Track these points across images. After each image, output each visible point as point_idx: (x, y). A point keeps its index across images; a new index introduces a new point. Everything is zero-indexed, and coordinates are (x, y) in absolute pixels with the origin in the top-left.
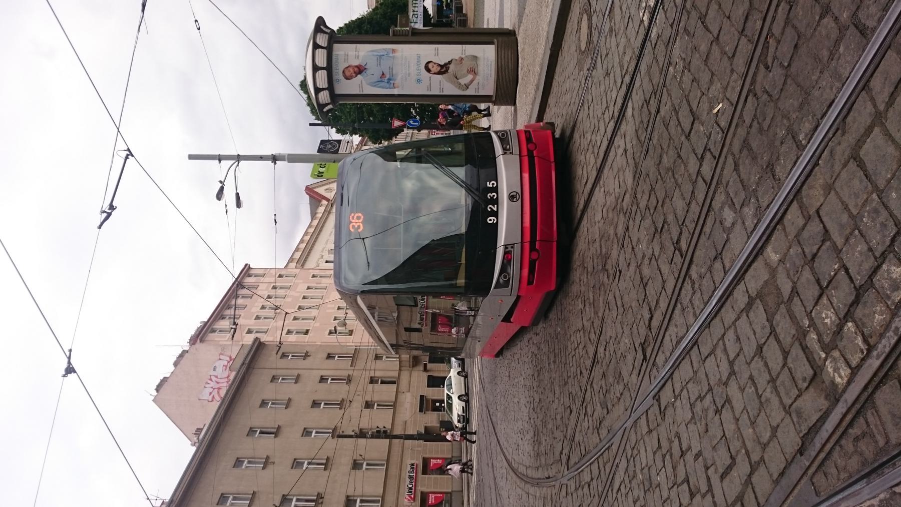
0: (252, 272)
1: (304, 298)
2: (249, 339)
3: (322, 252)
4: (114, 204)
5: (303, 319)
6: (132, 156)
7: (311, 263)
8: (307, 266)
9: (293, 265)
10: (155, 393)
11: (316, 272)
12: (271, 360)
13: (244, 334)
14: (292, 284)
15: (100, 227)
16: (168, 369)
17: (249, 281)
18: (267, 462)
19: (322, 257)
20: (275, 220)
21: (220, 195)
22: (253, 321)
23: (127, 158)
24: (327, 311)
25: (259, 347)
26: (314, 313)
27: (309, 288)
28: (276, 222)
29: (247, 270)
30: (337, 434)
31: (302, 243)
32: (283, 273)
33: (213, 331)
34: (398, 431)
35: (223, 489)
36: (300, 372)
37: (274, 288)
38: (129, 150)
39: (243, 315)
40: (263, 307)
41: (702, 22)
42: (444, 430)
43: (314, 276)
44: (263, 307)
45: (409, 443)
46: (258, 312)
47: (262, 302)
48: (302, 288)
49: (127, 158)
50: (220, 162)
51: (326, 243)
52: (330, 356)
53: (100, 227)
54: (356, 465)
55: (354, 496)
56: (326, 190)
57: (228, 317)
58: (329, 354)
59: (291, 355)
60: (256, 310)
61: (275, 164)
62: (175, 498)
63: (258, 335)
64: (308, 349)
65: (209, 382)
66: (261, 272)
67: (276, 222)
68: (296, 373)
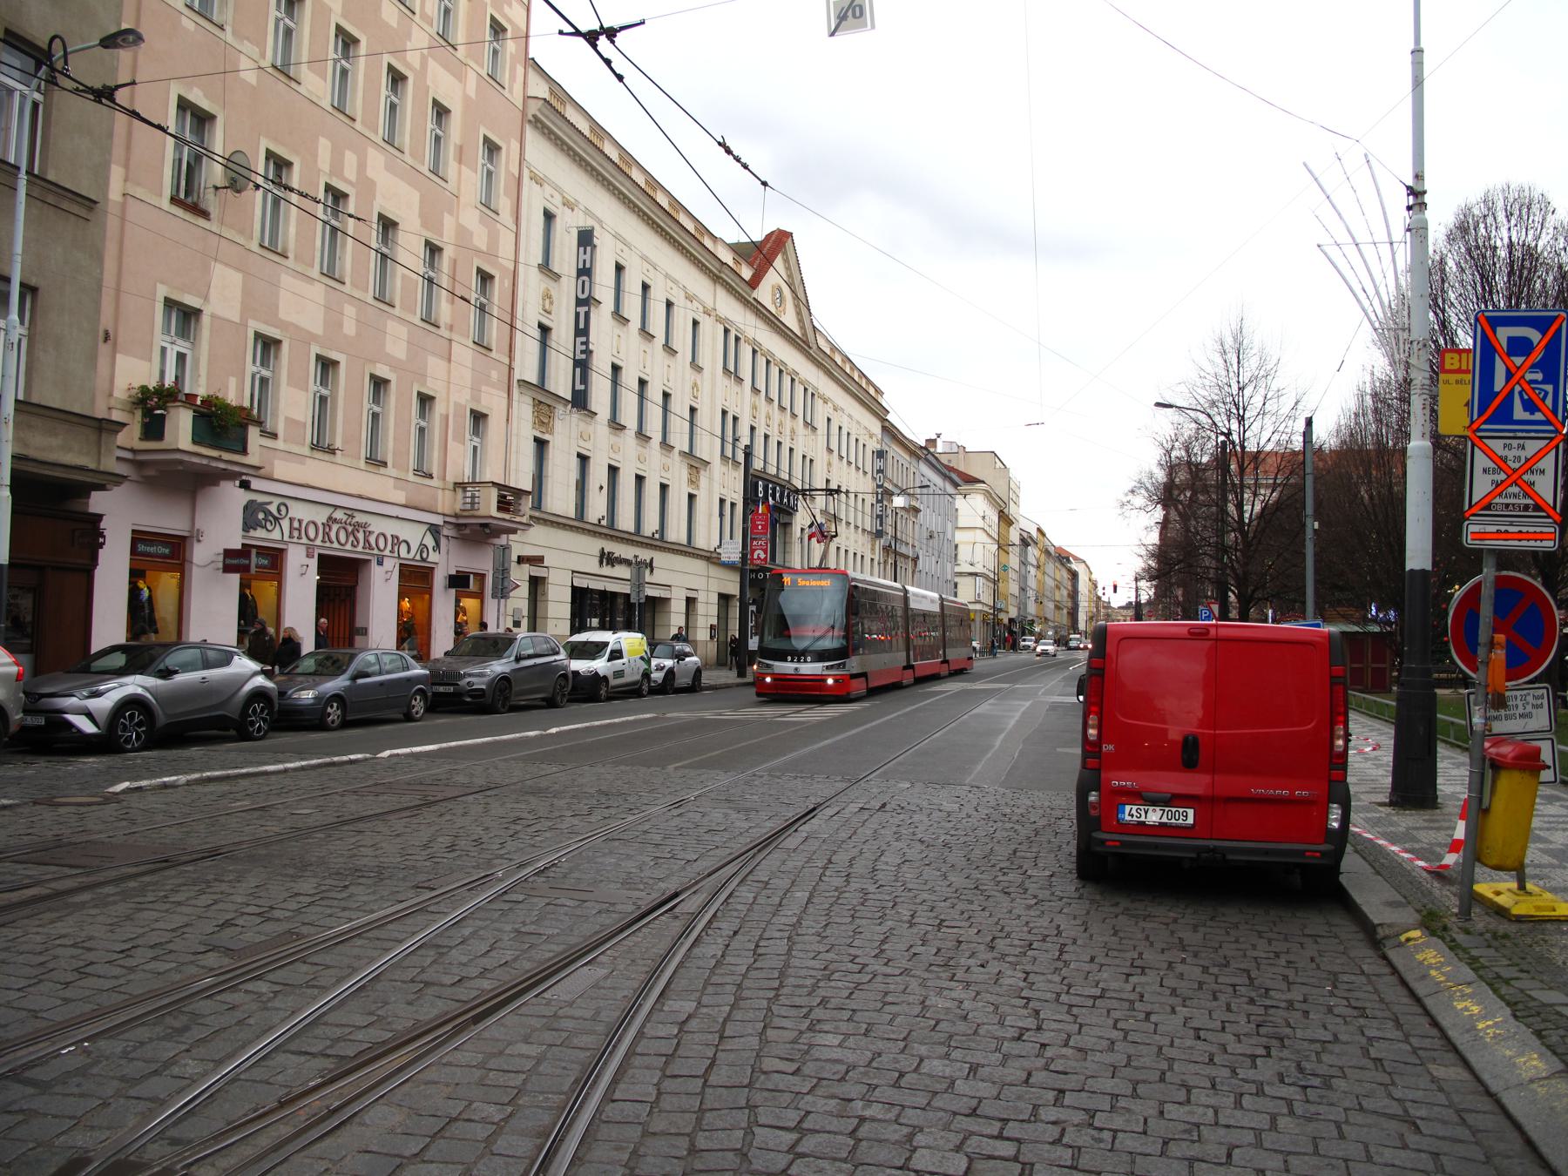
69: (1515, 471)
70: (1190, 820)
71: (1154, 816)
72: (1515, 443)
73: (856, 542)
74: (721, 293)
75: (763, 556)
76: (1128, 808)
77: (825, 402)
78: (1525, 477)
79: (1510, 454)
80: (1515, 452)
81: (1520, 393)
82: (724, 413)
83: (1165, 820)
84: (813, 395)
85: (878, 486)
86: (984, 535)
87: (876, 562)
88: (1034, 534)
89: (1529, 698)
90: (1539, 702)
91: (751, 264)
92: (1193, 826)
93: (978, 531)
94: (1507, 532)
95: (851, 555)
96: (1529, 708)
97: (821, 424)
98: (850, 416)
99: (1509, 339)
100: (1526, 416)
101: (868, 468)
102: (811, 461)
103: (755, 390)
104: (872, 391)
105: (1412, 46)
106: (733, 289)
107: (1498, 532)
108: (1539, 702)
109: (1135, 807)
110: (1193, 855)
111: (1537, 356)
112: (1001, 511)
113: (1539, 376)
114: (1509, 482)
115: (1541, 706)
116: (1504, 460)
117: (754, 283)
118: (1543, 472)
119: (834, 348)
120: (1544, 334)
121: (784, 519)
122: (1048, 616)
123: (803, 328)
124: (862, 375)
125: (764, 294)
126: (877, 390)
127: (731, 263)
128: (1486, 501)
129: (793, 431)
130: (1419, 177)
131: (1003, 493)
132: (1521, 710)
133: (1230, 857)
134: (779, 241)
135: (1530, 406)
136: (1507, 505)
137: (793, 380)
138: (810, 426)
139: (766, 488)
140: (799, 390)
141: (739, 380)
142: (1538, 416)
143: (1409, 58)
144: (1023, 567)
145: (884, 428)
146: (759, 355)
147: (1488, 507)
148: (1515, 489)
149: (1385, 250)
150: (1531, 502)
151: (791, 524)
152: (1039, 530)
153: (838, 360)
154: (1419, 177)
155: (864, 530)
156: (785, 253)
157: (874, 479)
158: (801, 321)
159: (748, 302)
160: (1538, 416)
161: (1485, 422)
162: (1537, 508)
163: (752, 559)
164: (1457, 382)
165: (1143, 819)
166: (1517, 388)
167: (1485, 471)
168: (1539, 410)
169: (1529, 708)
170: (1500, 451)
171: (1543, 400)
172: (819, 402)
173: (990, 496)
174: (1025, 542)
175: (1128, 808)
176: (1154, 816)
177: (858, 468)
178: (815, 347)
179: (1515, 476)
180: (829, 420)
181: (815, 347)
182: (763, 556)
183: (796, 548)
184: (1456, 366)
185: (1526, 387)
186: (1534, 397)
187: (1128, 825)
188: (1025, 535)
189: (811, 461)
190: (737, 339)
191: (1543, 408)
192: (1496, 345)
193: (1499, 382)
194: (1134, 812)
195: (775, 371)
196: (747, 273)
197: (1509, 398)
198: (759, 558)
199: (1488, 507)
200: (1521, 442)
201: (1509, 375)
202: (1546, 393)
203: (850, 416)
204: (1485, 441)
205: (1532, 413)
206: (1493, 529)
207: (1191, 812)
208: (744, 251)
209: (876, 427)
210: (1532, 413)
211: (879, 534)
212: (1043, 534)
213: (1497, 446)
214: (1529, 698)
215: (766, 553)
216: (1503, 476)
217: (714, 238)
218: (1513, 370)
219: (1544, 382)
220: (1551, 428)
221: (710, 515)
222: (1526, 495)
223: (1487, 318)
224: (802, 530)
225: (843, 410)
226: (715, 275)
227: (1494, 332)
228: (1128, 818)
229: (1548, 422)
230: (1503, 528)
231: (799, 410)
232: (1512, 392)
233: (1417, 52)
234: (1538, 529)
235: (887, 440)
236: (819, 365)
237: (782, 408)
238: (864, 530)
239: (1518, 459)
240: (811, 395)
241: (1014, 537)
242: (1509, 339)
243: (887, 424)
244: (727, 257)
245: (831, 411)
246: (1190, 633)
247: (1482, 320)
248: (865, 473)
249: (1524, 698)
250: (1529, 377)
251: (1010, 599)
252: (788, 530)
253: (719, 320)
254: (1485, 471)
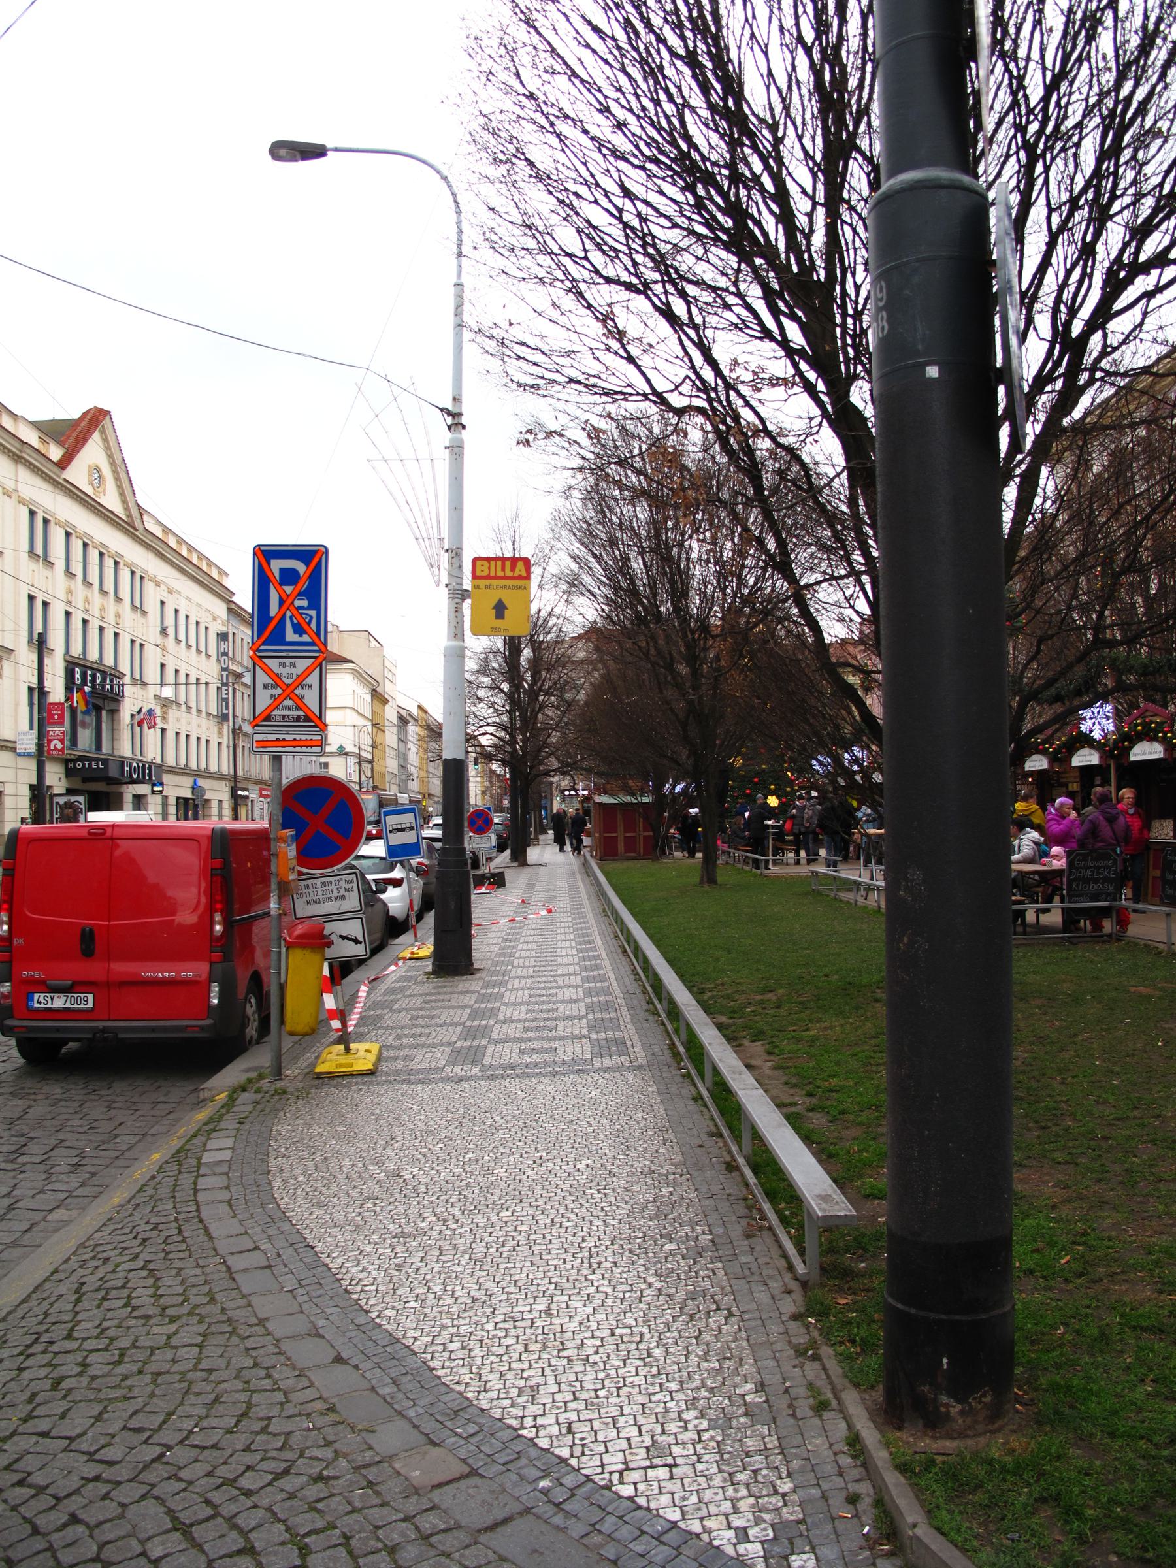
69: (288, 686)
70: (90, 1005)
71: (60, 1002)
72: (288, 661)
73: (199, 726)
74: (24, 474)
75: (60, 746)
76: (36, 996)
77: (158, 584)
78: (297, 692)
79: (284, 672)
80: (288, 670)
81: (291, 618)
82: (31, 598)
83: (68, 1005)
84: (142, 578)
85: (223, 669)
86: (355, 714)
87: (224, 747)
88: (415, 711)
89: (342, 883)
90: (350, 886)
91: (61, 443)
92: (92, 1010)
93: (348, 711)
94: (284, 740)
95: (183, 738)
96: (342, 892)
97: (152, 606)
98: (188, 599)
99: (282, 571)
100: (296, 638)
101: (213, 651)
103: (69, 573)
104: (214, 574)
105: (455, 280)
106: (39, 469)
107: (278, 740)
108: (350, 886)
109: (42, 995)
110: (90, 1036)
111: (304, 585)
112: (374, 690)
113: (305, 603)
114: (285, 695)
115: (352, 889)
116: (279, 676)
117: (63, 464)
118: (310, 687)
119: (167, 530)
120: (307, 564)
121: (112, 706)
122: (433, 792)
123: (127, 509)
124: (201, 556)
125: (77, 474)
126: (222, 572)
127: (35, 443)
128: (267, 712)
129: (118, 615)
130: (456, 400)
131: (374, 671)
132: (335, 894)
133: (121, 1036)
134: (96, 419)
135: (299, 629)
136: (283, 716)
137: (116, 563)
138: (139, 609)
139: (84, 675)
140: (125, 575)
141: (49, 564)
142: (306, 638)
143: (452, 289)
144: (402, 745)
145: (230, 610)
146: (73, 539)
147: (268, 718)
148: (288, 702)
149: (426, 465)
150: (301, 713)
151: (118, 710)
152: (420, 707)
153: (172, 542)
154: (456, 400)
155: (208, 714)
156: (103, 432)
157: (219, 661)
158: (124, 501)
159: (58, 483)
160: (306, 638)
161: (263, 644)
162: (307, 719)
163: (49, 750)
164: (486, 587)
165: (49, 1005)
166: (288, 614)
167: (265, 686)
168: (306, 633)
169: (342, 892)
170: (277, 670)
171: (309, 624)
172: (149, 586)
173: (361, 676)
174: (403, 720)
175: (36, 996)
176: (60, 1002)
177: (199, 651)
178: (141, 529)
179: (288, 691)
180: (162, 603)
181: (141, 529)
182: (60, 746)
183: (125, 735)
184: (486, 573)
185: (295, 612)
186: (301, 621)
187: (38, 1010)
188: (404, 713)
190: (46, 522)
191: (309, 631)
192: (269, 574)
193: (274, 609)
194: (41, 999)
195: (94, 555)
196: (55, 453)
197: (283, 619)
198: (56, 749)
199: (268, 718)
200: (292, 660)
201: (282, 602)
202: (311, 618)
203: (188, 599)
204: (265, 660)
205: (301, 636)
206: (273, 737)
207: (90, 997)
208: (50, 430)
209: (221, 609)
210: (301, 636)
211: (224, 718)
212: (425, 712)
213: (273, 664)
214: (342, 883)
215: (62, 741)
216: (279, 691)
217: (14, 416)
218: (285, 598)
219: (308, 608)
220: (316, 648)
221: (17, 705)
222: (298, 708)
223: (263, 552)
224: (132, 716)
225: (179, 593)
226: (14, 454)
227: (269, 564)
228: (36, 1005)
229: (313, 644)
230: (281, 737)
231: (125, 593)
232: (284, 615)
233: (459, 285)
234: (309, 737)
235: (234, 622)
236: (148, 547)
237: (103, 592)
238: (208, 714)
239: (290, 675)
240: (139, 578)
241: (391, 713)
242: (282, 571)
243: (233, 606)
244: (31, 437)
245: (165, 594)
246: (89, 833)
247: (259, 553)
248: (208, 656)
249: (337, 883)
250: (297, 603)
251: (388, 778)
252: (116, 717)
253: (22, 502)
254: (265, 686)
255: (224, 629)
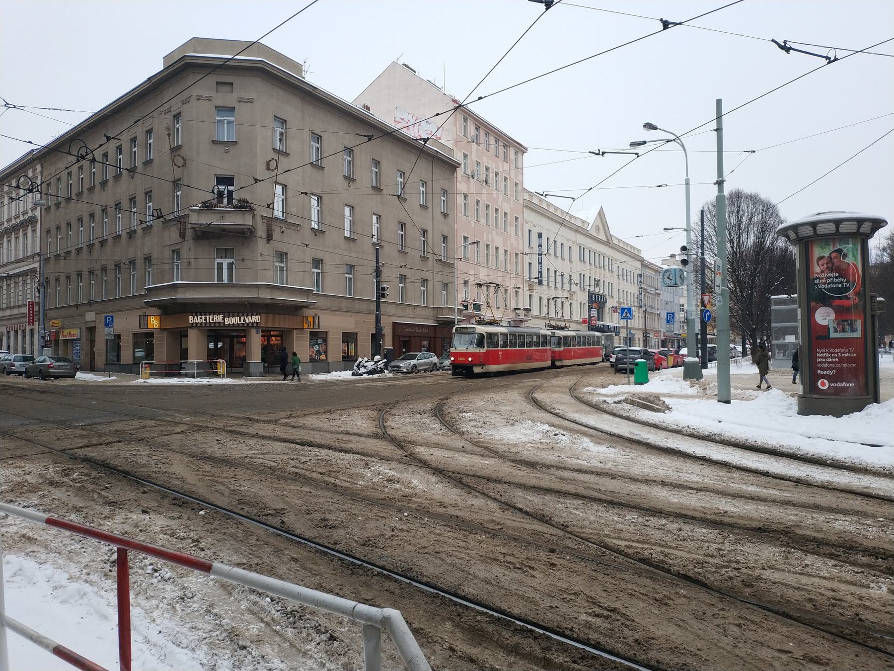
0: (520, 154)
1: (497, 210)
2: (458, 157)
3: (539, 226)
4: (791, 51)
5: (477, 209)
6: (828, 63)
7: (529, 215)
8: (526, 211)
9: (526, 197)
10: (400, 62)
11: (520, 221)
12: (440, 182)
13: (463, 151)
14: (509, 197)
15: (773, 41)
16: (424, 73)
17: (512, 151)
18: (350, 179)
19: (534, 226)
20: (661, 186)
21: (649, 126)
22: (475, 159)
23: (827, 58)
24: (485, 234)
25: (451, 167)
26: (483, 221)
27: (506, 214)
28: (659, 186)
29: (521, 149)
30: (377, 249)
31: (547, 205)
32: (519, 187)
33: (465, 120)
34: (383, 308)
35: (325, 137)
36: (430, 208)
37: (506, 179)
38: (836, 59)
39: (480, 148)
40: (487, 169)
41: (719, 625)
42: (385, 353)
43: (516, 218)
44: (487, 169)
45: (373, 319)
46: (483, 163)
47: (492, 167)
48: (506, 207)
49: (827, 58)
50: (715, 130)
51: (547, 230)
52: (445, 238)
53: (773, 41)
54: (351, 268)
55: (286, 262)
56: (598, 226)
57: (477, 133)
58: (447, 237)
59: (445, 199)
60: (485, 161)
61: (715, 184)
62: (317, 91)
63: (462, 166)
64: (451, 216)
65: (415, 118)
66: (520, 165)
67: (659, 186)
68: (430, 205)
102: (584, 275)
172: (614, 262)
189: (584, 275)
209: (638, 264)
255: (640, 273)
